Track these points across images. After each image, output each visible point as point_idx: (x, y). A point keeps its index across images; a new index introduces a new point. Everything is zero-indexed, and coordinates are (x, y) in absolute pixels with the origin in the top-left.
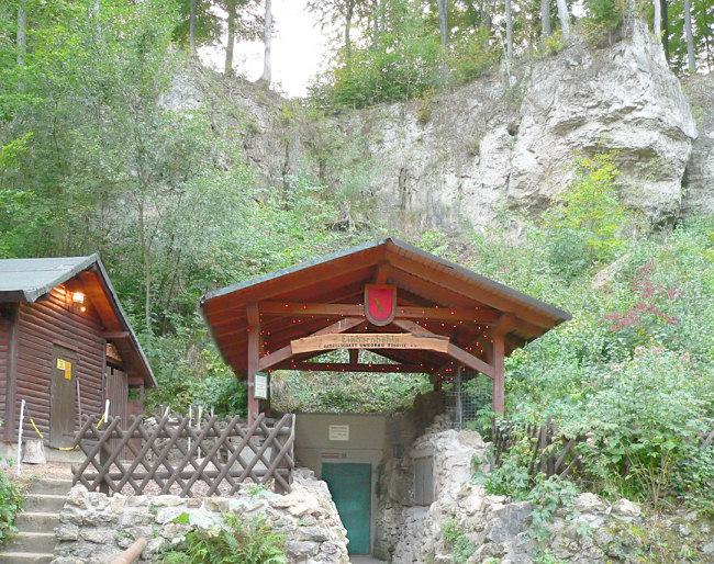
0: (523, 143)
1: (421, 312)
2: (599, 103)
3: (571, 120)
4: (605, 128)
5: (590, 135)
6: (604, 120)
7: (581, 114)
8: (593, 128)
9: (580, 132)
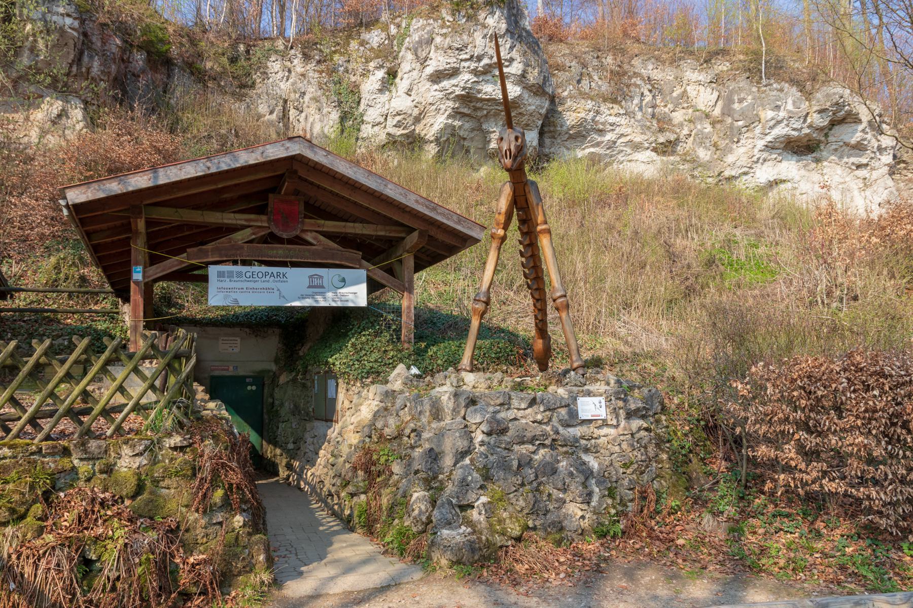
0: (402, 84)
1: (331, 226)
2: (472, 56)
3: (445, 70)
4: (475, 79)
5: (462, 84)
6: (475, 72)
7: (455, 65)
8: (465, 77)
9: (454, 81)
